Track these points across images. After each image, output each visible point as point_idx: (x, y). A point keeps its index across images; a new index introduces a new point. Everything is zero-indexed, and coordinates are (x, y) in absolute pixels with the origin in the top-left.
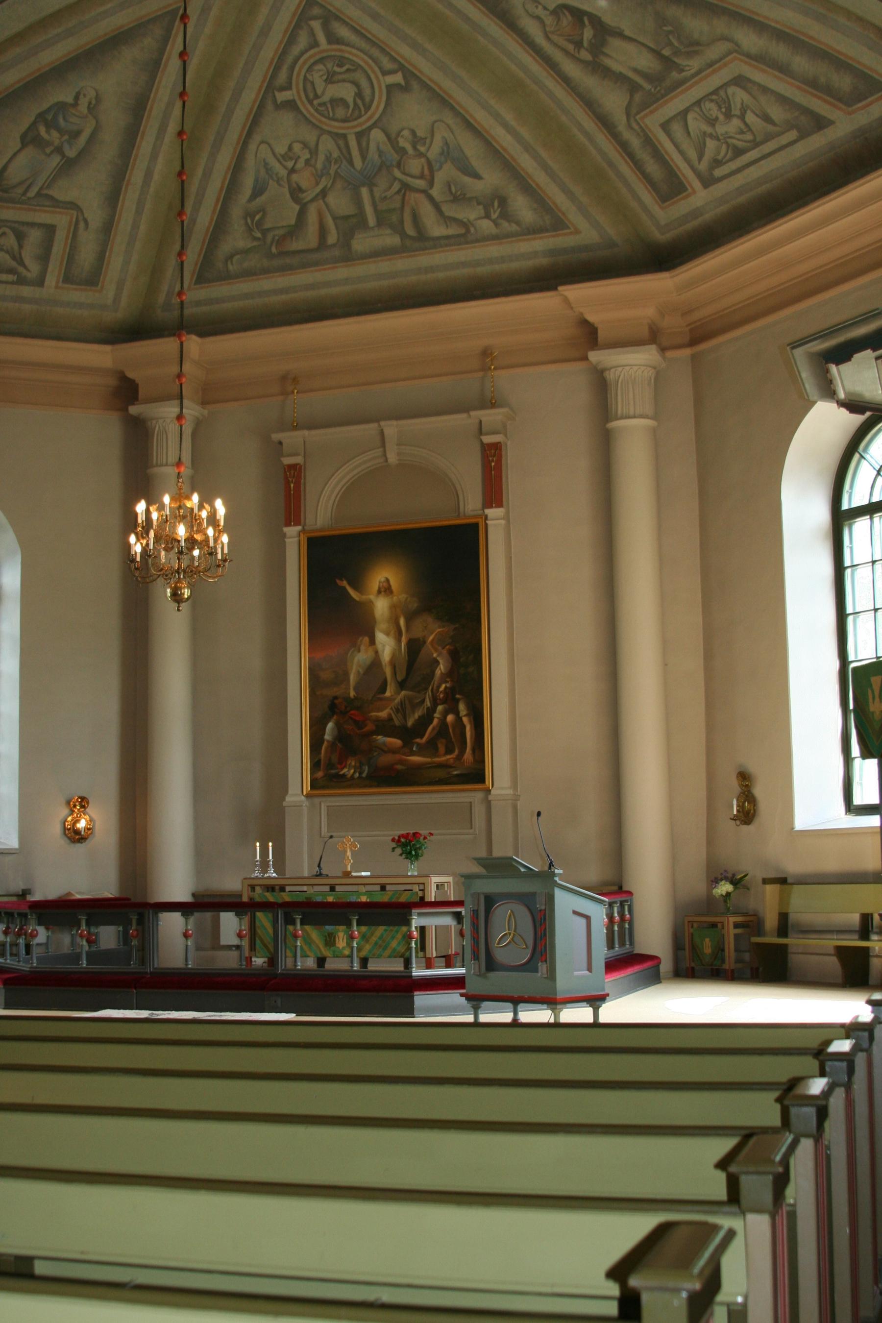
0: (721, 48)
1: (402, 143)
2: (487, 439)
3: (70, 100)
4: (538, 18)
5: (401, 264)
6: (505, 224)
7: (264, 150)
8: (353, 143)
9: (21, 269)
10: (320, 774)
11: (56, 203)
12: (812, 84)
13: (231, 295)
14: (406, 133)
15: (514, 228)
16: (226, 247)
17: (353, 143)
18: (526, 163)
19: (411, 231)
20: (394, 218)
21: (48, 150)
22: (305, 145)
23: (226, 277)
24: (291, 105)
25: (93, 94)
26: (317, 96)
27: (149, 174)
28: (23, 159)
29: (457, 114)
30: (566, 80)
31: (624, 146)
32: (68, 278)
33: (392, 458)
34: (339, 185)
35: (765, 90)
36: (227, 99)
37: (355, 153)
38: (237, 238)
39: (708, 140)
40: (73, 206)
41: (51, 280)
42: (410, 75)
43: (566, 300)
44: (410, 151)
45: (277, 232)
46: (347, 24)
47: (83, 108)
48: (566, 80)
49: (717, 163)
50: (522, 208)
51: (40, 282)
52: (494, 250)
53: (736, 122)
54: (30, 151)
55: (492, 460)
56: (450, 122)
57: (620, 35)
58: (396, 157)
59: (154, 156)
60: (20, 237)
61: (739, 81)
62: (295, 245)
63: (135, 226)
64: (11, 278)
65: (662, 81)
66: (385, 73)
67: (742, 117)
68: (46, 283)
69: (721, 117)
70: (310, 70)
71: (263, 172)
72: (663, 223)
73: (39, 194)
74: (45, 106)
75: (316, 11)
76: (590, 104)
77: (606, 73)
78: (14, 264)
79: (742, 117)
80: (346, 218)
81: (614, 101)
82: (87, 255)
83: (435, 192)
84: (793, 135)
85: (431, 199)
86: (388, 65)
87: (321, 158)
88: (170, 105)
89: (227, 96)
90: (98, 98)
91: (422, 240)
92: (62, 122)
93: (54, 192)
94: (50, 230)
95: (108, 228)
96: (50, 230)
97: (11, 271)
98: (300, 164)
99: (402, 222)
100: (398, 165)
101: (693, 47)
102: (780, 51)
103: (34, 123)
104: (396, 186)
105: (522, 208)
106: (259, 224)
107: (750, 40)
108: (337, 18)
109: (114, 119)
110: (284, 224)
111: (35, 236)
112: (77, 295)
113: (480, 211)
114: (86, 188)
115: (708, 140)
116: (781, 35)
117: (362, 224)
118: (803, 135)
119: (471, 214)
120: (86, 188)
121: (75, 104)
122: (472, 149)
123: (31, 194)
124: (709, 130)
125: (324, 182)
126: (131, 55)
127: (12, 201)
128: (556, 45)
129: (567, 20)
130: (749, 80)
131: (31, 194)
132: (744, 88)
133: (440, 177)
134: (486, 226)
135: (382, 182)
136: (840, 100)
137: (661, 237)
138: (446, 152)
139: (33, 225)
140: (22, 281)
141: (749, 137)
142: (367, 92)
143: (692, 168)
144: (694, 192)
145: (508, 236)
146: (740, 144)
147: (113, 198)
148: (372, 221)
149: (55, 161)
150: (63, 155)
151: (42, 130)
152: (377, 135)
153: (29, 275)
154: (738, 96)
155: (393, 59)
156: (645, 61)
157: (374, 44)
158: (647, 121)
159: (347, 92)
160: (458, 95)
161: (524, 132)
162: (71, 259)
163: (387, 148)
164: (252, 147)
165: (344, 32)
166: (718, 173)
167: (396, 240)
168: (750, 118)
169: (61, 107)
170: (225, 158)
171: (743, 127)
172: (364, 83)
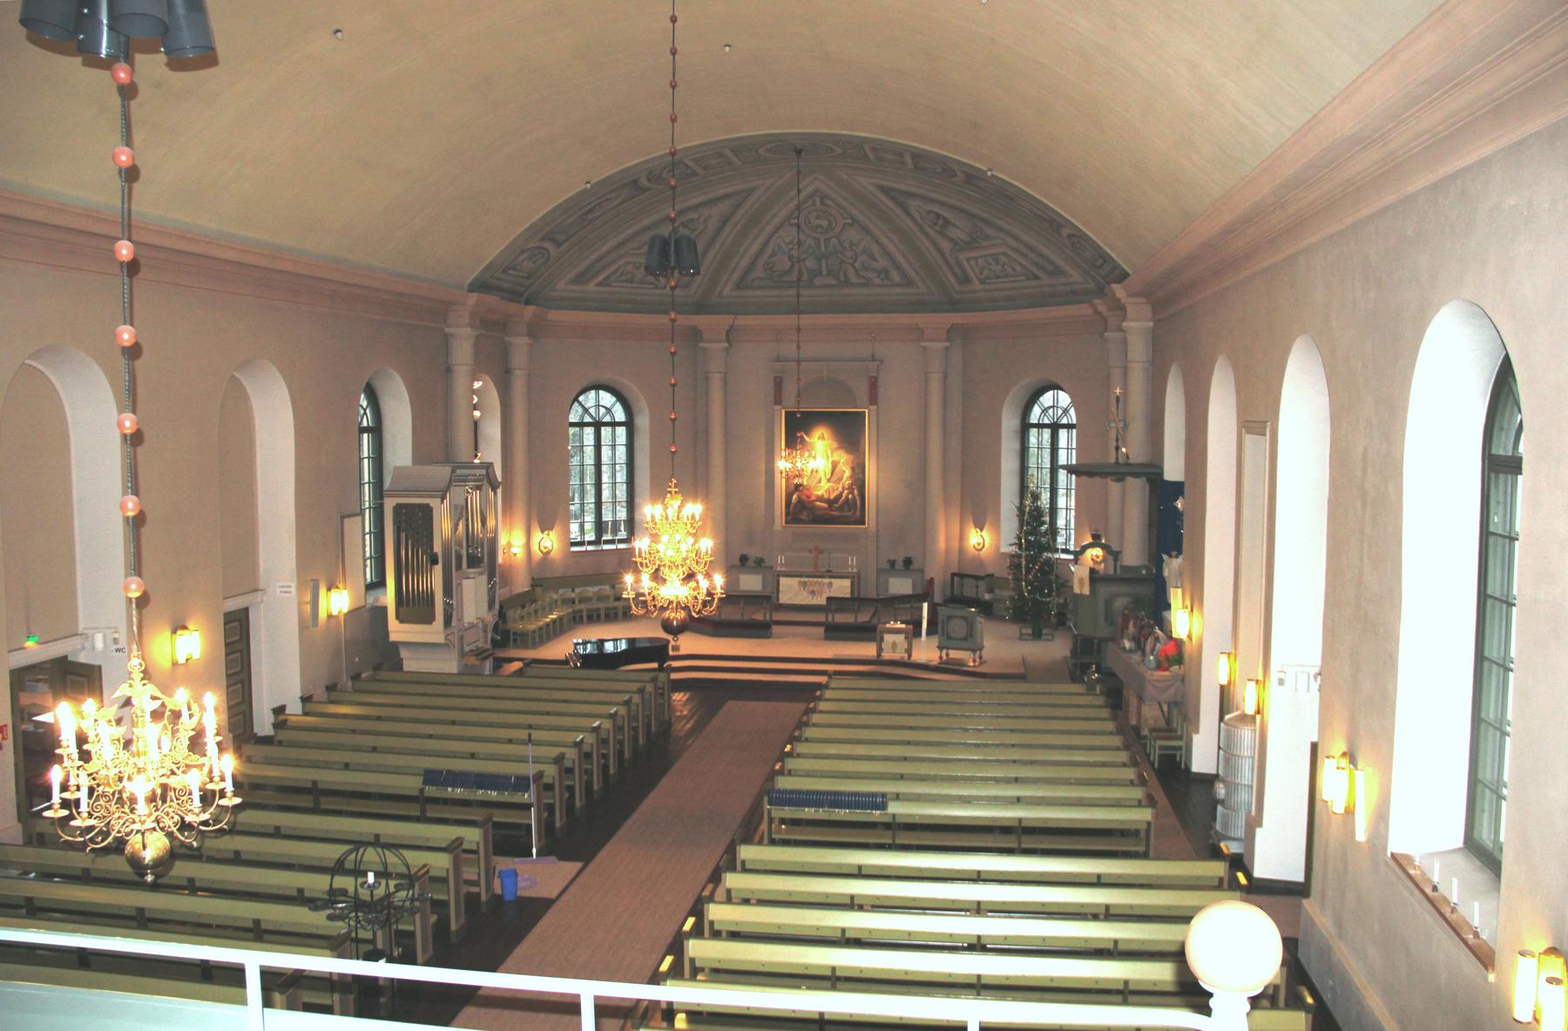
12: (1037, 265)
18: (901, 259)
31: (947, 262)
38: (759, 272)
42: (854, 220)
48: (925, 233)
55: (873, 386)
61: (1005, 254)
77: (945, 236)
91: (847, 283)
101: (987, 237)
116: (1026, 245)
117: (820, 273)
119: (870, 275)
122: (876, 250)
134: (877, 281)
140: (657, 287)
154: (1003, 259)
156: (964, 236)
159: (825, 223)
165: (829, 202)
169: (692, 220)
170: (760, 240)
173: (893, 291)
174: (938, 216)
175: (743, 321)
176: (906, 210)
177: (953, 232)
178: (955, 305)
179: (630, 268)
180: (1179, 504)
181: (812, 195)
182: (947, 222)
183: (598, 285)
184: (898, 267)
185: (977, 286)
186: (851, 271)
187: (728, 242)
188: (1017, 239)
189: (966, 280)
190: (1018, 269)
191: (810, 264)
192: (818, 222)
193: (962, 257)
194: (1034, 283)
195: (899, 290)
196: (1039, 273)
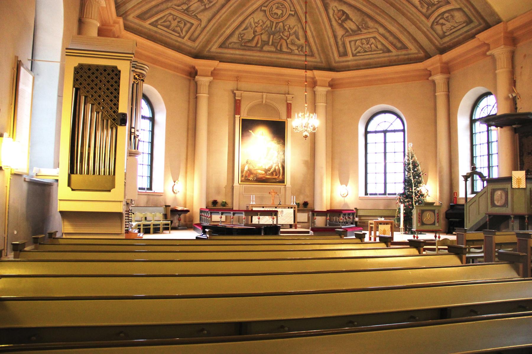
0: (374, 30)
1: (286, 28)
2: (288, 102)
4: (334, 11)
5: (273, 55)
7: (252, 20)
8: (274, 24)
10: (243, 179)
13: (228, 53)
17: (274, 24)
19: (279, 48)
22: (263, 21)
24: (265, 11)
27: (220, 17)
30: (331, 25)
32: (189, 39)
33: (264, 102)
35: (379, 41)
38: (234, 39)
40: (200, 20)
41: (186, 38)
42: (296, 12)
43: (314, 74)
48: (331, 25)
49: (359, 52)
51: (183, 38)
52: (296, 58)
53: (369, 46)
54: (199, 3)
57: (352, 20)
60: (185, 24)
61: (374, 38)
62: (249, 45)
64: (178, 35)
65: (354, 33)
66: (291, 11)
67: (371, 45)
71: (249, 25)
73: (195, 15)
76: (334, 32)
79: (371, 45)
81: (340, 33)
82: (196, 34)
83: (288, 41)
84: (381, 52)
85: (287, 42)
86: (292, 9)
87: (265, 25)
91: (281, 51)
97: (179, 33)
98: (259, 26)
101: (367, 28)
102: (387, 35)
104: (280, 37)
107: (381, 30)
111: (188, 25)
113: (297, 48)
116: (389, 32)
119: (294, 48)
120: (205, 17)
122: (301, 33)
124: (361, 45)
125: (263, 31)
127: (188, 15)
129: (341, 13)
133: (291, 38)
135: (277, 35)
137: (334, 64)
140: (180, 37)
142: (284, 13)
147: (210, 21)
148: (270, 43)
149: (203, 7)
152: (281, 24)
154: (372, 40)
155: (294, 8)
156: (354, 27)
157: (292, 3)
159: (279, 12)
162: (192, 34)
163: (282, 28)
164: (249, 18)
166: (358, 54)
167: (274, 50)
168: (373, 46)
170: (241, 19)
174: (344, 13)
177: (349, 25)
178: (331, 69)
179: (170, 18)
180: (15, 232)
182: (348, 18)
183: (150, 24)
185: (350, 57)
186: (284, 45)
188: (385, 28)
189: (345, 54)
190: (380, 46)
191: (264, 37)
192: (276, 11)
193: (347, 40)
194: (387, 54)
196: (390, 48)
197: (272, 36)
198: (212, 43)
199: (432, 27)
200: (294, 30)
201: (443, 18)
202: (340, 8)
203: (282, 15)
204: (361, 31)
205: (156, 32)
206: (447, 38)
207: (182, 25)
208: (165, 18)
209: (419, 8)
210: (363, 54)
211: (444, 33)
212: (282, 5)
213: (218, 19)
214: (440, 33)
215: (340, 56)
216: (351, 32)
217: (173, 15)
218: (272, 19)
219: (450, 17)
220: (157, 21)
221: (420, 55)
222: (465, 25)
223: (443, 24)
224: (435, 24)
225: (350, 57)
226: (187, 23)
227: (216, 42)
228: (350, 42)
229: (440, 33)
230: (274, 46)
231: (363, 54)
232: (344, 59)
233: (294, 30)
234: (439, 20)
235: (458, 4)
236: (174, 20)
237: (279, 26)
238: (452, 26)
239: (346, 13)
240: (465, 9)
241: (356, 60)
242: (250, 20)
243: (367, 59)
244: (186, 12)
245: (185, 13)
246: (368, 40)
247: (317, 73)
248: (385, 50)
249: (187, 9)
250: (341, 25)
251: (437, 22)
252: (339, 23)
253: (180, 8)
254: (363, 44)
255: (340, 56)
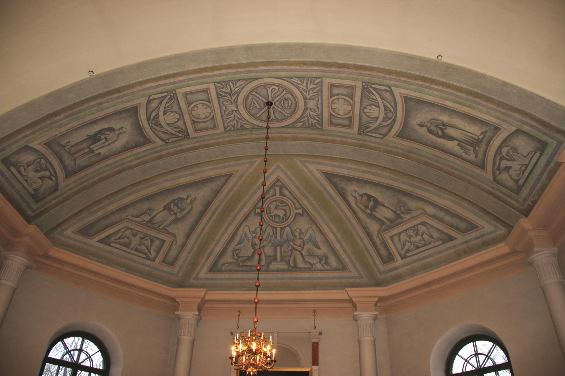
0: (420, 212)
1: (296, 233)
3: (185, 197)
4: (355, 197)
6: (326, 266)
9: (149, 254)
11: (168, 233)
12: (451, 226)
14: (298, 230)
15: (329, 268)
16: (223, 261)
18: (337, 246)
19: (292, 264)
20: (287, 259)
21: (172, 213)
23: (221, 271)
25: (193, 196)
26: (270, 213)
27: (203, 229)
28: (162, 214)
29: (317, 226)
30: (358, 219)
34: (270, 244)
35: (432, 227)
36: (238, 209)
37: (278, 234)
38: (228, 258)
39: (407, 243)
40: (174, 235)
41: (158, 260)
44: (298, 236)
45: (243, 258)
46: (288, 189)
47: (188, 201)
48: (358, 219)
49: (409, 251)
50: (333, 261)
51: (154, 260)
52: (320, 275)
53: (419, 237)
56: (314, 228)
57: (383, 205)
58: (292, 238)
59: (207, 224)
60: (152, 242)
61: (424, 224)
62: (249, 263)
63: (193, 247)
65: (393, 223)
66: (296, 209)
67: (422, 236)
68: (156, 261)
69: (414, 235)
70: (270, 203)
71: (244, 236)
72: (382, 271)
73: (163, 228)
74: (176, 197)
75: (279, 183)
76: (365, 228)
78: (147, 251)
79: (422, 236)
80: (270, 256)
81: (374, 227)
82: (173, 254)
83: (303, 252)
84: (440, 242)
85: (301, 254)
86: (298, 206)
87: (266, 234)
88: (258, 188)
89: (239, 207)
90: (195, 199)
91: (296, 268)
92: (180, 205)
93: (169, 229)
94: (163, 242)
95: (183, 245)
96: (163, 242)
97: (145, 254)
99: (289, 261)
100: (293, 241)
101: (409, 211)
102: (441, 214)
103: (171, 202)
104: (290, 248)
105: (333, 261)
106: (237, 254)
107: (430, 210)
108: (285, 187)
109: (198, 207)
110: (247, 255)
111: (157, 243)
112: (165, 268)
113: (318, 260)
114: (180, 230)
115: (407, 243)
116: (442, 209)
118: (444, 242)
119: (314, 261)
120: (180, 230)
121: (186, 199)
122: (319, 239)
123: (161, 227)
124: (407, 239)
126: (212, 186)
127: (153, 228)
128: (358, 207)
129: (365, 198)
130: (427, 223)
131: (161, 227)
132: (425, 226)
133: (306, 247)
134: (319, 266)
135: (285, 246)
136: (460, 231)
138: (310, 239)
139: (158, 238)
140: (148, 258)
141: (423, 242)
142: (288, 214)
143: (398, 252)
144: (397, 260)
145: (326, 270)
146: (419, 245)
147: (188, 236)
148: (279, 259)
149: (173, 217)
150: (176, 216)
151: (172, 205)
152: (288, 229)
153: (151, 256)
154: (422, 228)
155: (300, 204)
156: (390, 215)
158: (385, 235)
159: (281, 213)
160: (319, 220)
161: (339, 236)
162: (167, 254)
164: (242, 227)
165: (286, 192)
166: (408, 254)
168: (425, 236)
169: (182, 199)
170: (231, 229)
171: (421, 239)
172: (288, 211)
173: (331, 275)
174: (369, 197)
175: (212, 295)
176: (342, 194)
177: (383, 213)
179: (128, 233)
181: (273, 185)
182: (377, 203)
184: (335, 254)
185: (399, 262)
187: (207, 228)
188: (435, 205)
189: (390, 258)
192: (276, 212)
193: (387, 236)
194: (449, 244)
195: (336, 274)
197: (278, 248)
198: (199, 267)
199: (495, 180)
200: (308, 235)
201: (502, 158)
202: (361, 192)
203: (286, 217)
204: (402, 218)
205: (110, 252)
206: (524, 189)
207: (148, 243)
208: (120, 234)
209: (463, 155)
210: (414, 252)
211: (517, 181)
212: (282, 202)
213: (201, 233)
214: (511, 184)
215: (385, 262)
216: (388, 223)
217: (132, 229)
218: (274, 224)
219: (511, 151)
220: (108, 237)
221: (499, 233)
222: (538, 154)
223: (508, 169)
224: (497, 172)
225: (399, 262)
226: (154, 239)
227: (204, 264)
228: (391, 238)
229: (511, 184)
230: (285, 262)
231: (414, 252)
232: (391, 266)
233: (308, 235)
234: (499, 164)
235: (511, 124)
236: (135, 235)
237: (285, 233)
238: (522, 165)
239: (374, 197)
240: (526, 128)
241: (408, 264)
242: (244, 229)
243: (424, 258)
244: (149, 224)
245: (149, 227)
246: (415, 229)
247: (353, 292)
248: (445, 237)
249: (151, 221)
250: (372, 216)
251: (498, 169)
252: (368, 214)
253: (139, 219)
254: (410, 237)
255: (385, 262)
